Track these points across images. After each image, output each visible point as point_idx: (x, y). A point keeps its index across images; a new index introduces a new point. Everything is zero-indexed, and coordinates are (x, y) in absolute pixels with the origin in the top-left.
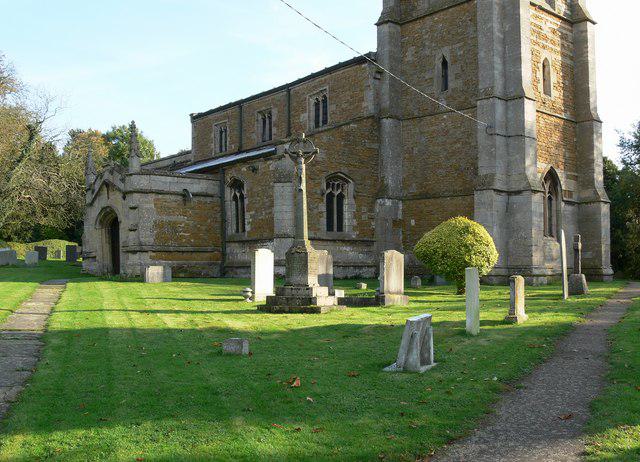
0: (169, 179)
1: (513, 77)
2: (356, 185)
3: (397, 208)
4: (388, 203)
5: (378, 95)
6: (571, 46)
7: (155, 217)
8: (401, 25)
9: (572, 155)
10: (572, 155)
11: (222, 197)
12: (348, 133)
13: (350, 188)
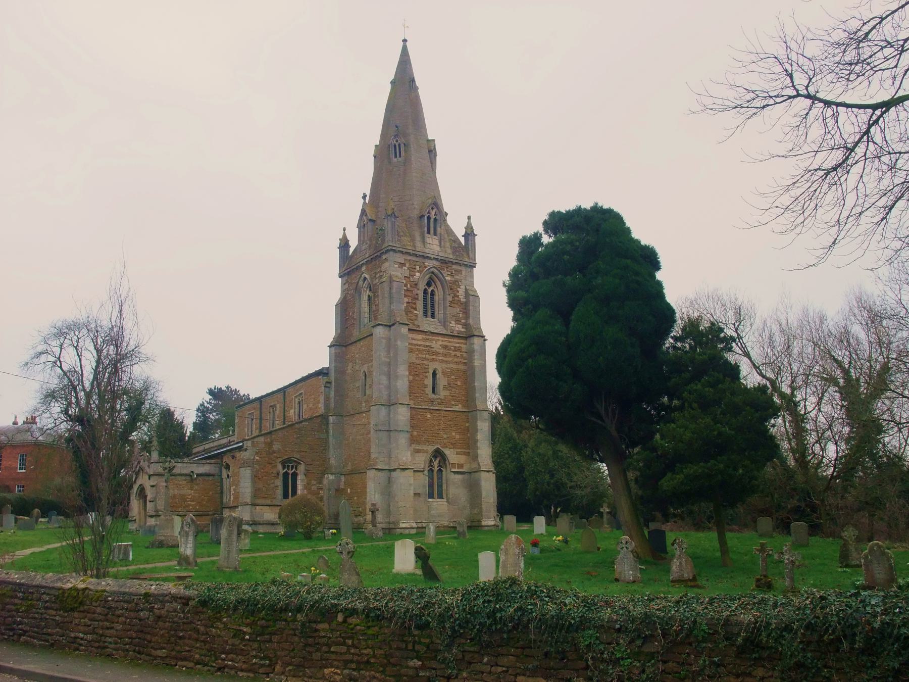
4: (331, 477)
5: (327, 399)
11: (221, 475)
13: (302, 468)
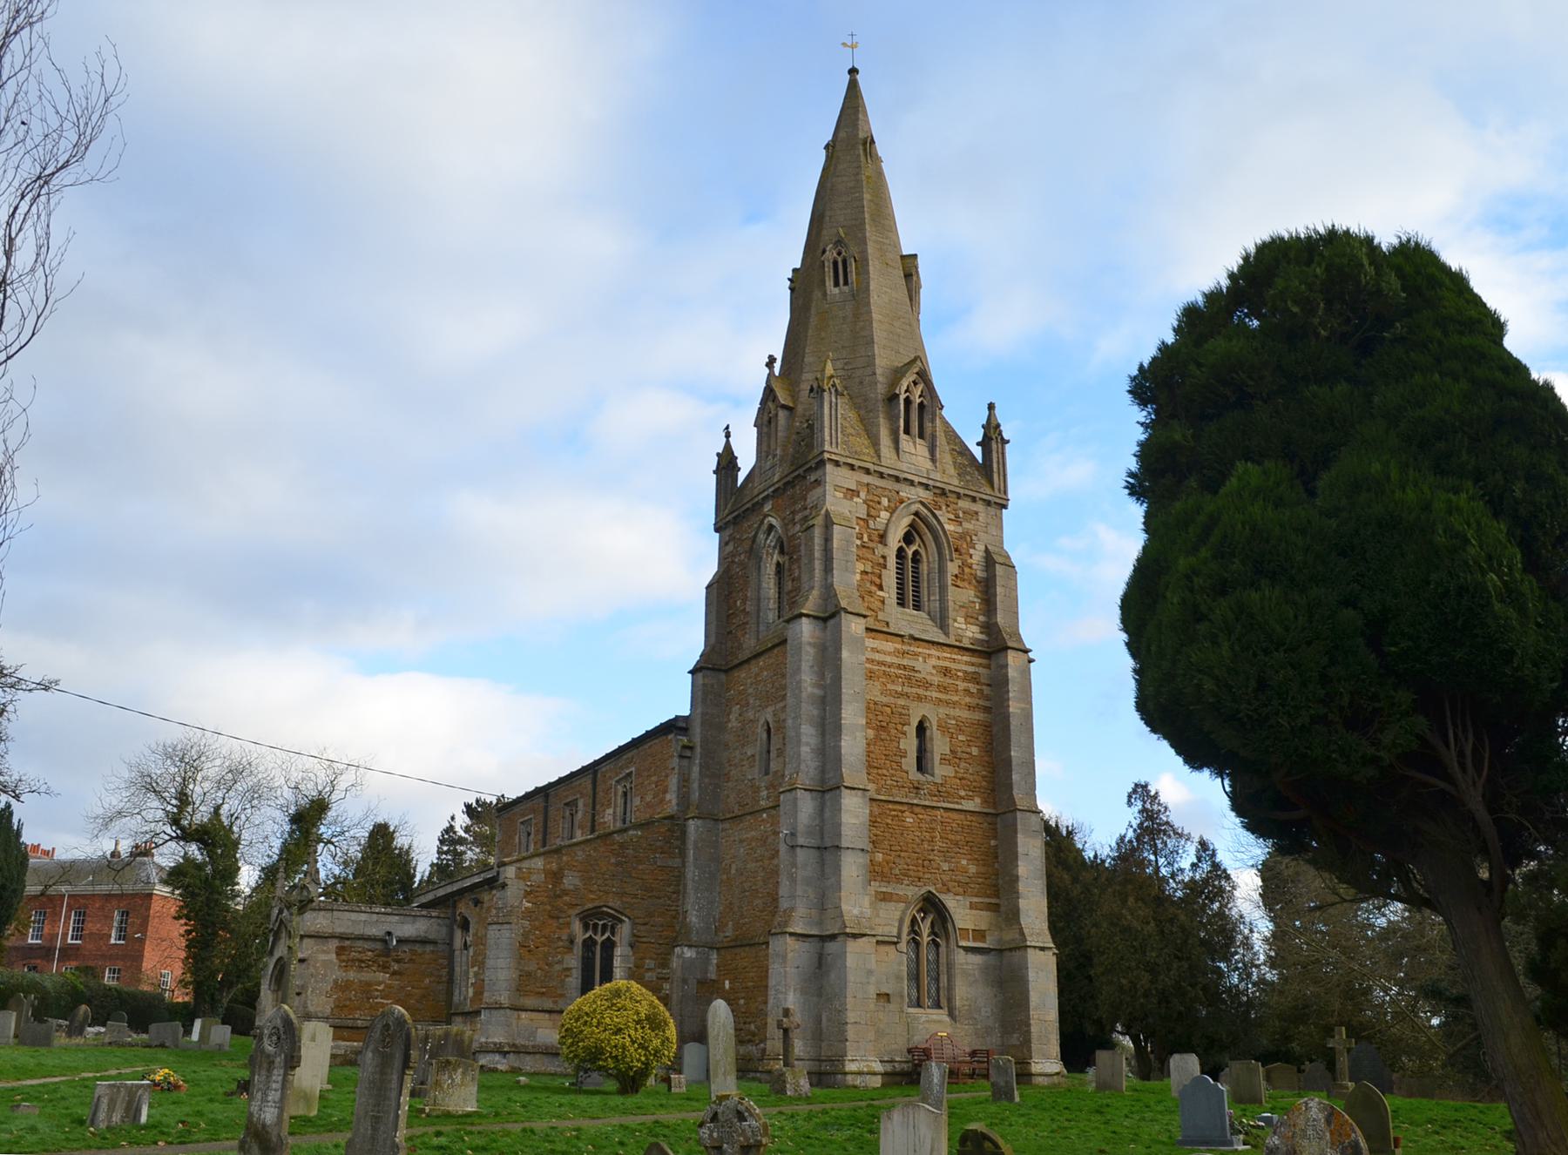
0: (363, 917)
1: (829, 755)
2: (634, 924)
3: (707, 961)
4: (689, 953)
5: (685, 781)
6: (986, 690)
7: (337, 974)
8: (726, 671)
9: (982, 869)
10: (982, 869)
12: (622, 846)
13: (624, 931)
